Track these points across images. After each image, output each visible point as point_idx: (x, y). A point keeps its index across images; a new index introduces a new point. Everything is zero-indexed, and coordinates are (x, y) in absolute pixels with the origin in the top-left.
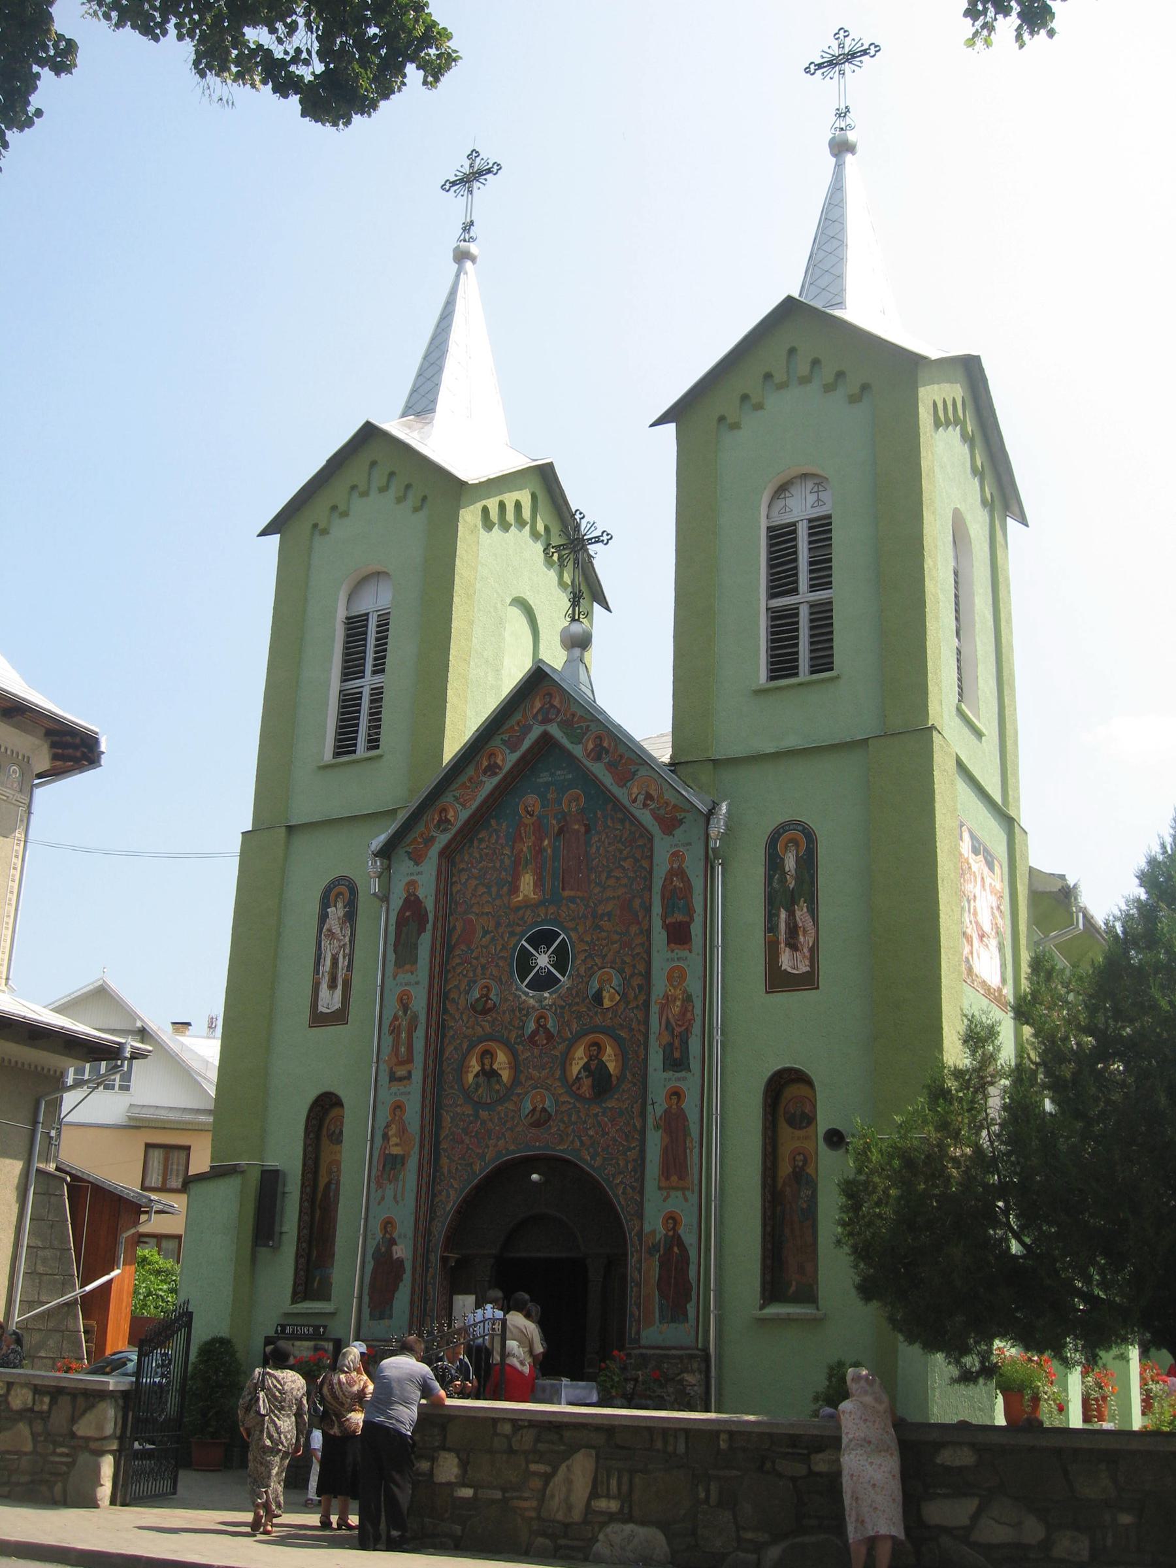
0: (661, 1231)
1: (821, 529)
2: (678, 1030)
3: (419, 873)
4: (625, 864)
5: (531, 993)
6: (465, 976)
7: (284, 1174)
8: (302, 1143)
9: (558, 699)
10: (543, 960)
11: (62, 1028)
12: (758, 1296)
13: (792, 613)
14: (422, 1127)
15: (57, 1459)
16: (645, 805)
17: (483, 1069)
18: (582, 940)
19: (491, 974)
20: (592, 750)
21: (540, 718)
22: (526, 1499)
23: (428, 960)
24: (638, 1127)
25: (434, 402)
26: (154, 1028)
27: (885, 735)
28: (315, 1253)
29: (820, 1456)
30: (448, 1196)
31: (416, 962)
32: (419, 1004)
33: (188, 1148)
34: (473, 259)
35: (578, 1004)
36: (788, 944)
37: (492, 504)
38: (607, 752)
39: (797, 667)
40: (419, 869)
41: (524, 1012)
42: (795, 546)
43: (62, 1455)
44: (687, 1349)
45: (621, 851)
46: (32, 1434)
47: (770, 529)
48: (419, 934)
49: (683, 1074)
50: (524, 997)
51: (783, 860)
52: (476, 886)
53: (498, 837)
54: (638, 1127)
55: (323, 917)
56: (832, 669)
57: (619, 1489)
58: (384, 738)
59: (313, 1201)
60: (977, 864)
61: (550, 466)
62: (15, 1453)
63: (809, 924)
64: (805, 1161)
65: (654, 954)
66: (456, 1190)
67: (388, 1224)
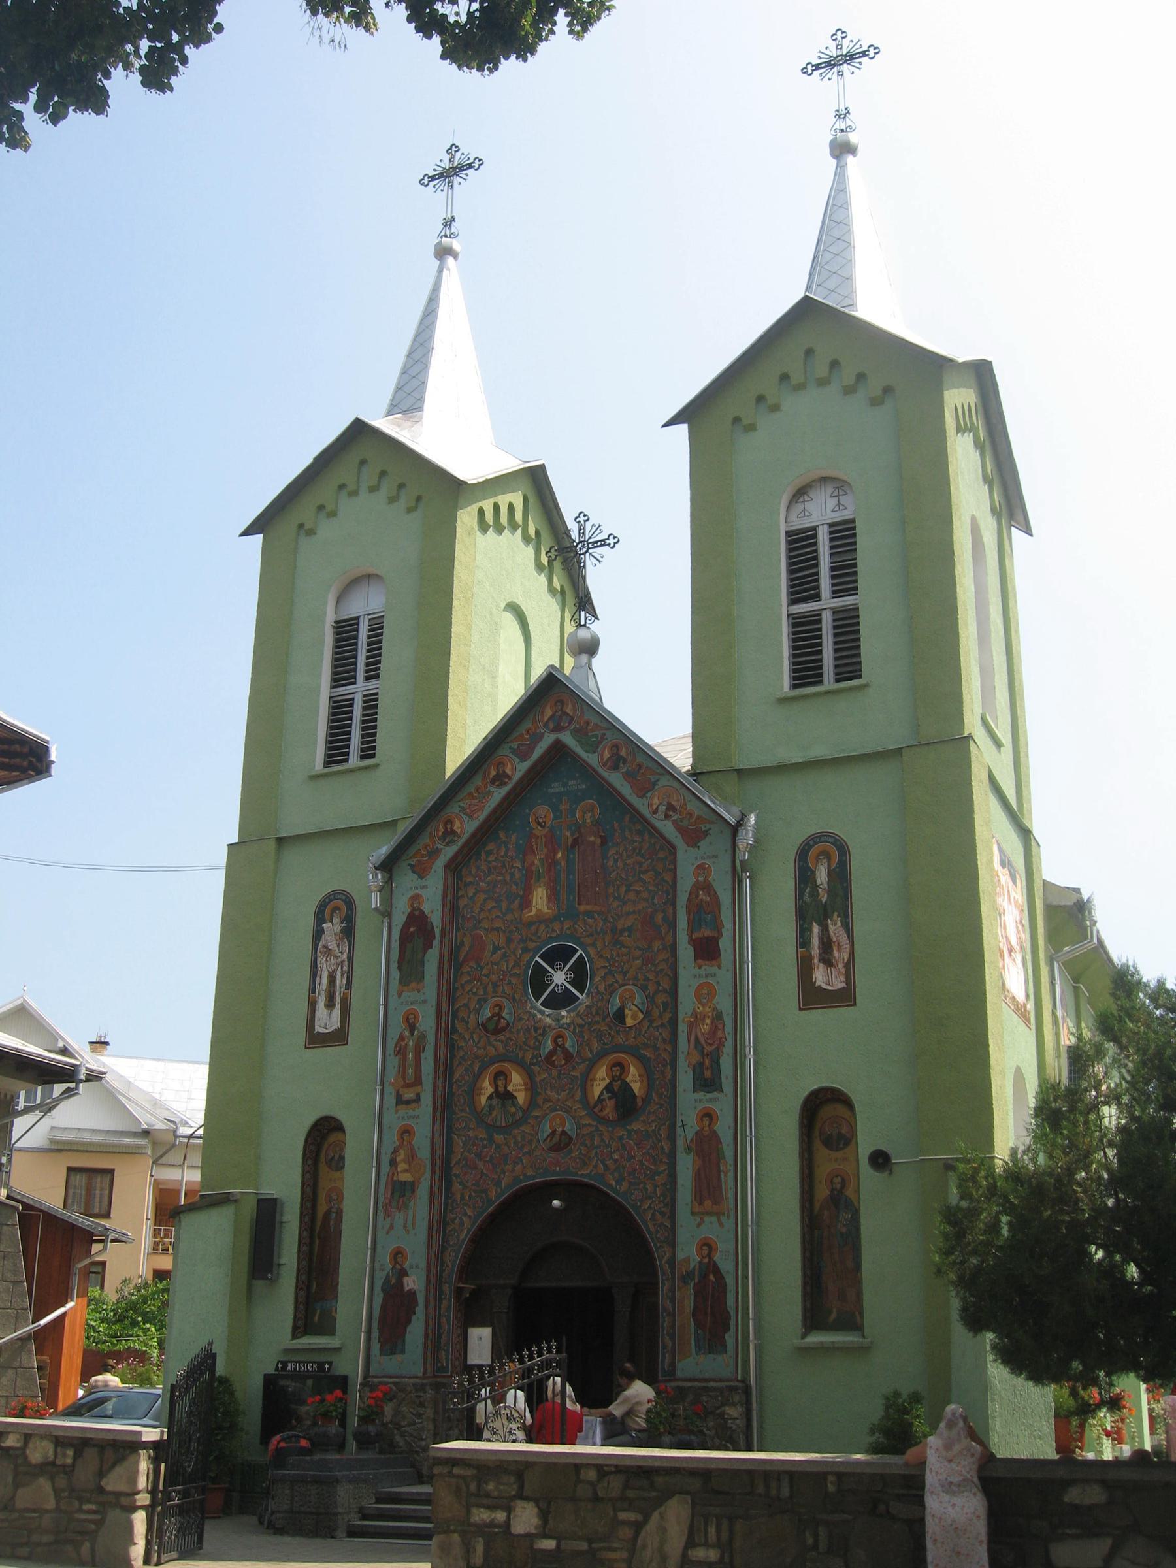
2: (708, 1049)
3: (423, 887)
5: (548, 1011)
6: (475, 994)
7: (282, 1204)
10: (559, 977)
11: (16, 1050)
13: (815, 619)
15: (84, 1516)
16: (667, 817)
18: (601, 956)
20: (609, 759)
21: (551, 725)
22: (615, 1550)
23: (435, 978)
24: (667, 1151)
25: (421, 400)
26: (76, 1047)
27: (919, 745)
31: (422, 979)
32: (427, 1024)
33: (111, 1172)
34: (455, 256)
35: (597, 1022)
37: (487, 505)
38: (625, 761)
39: (821, 675)
42: (816, 551)
43: (89, 1512)
44: (728, 1380)
45: (640, 864)
46: (55, 1490)
49: (716, 1094)
50: (539, 1016)
51: (814, 872)
52: (485, 899)
53: (507, 850)
54: (667, 1151)
55: (318, 933)
56: (860, 677)
59: (311, 1230)
60: (1004, 877)
62: (34, 1511)
63: (844, 938)
65: (681, 972)
67: (398, 1254)
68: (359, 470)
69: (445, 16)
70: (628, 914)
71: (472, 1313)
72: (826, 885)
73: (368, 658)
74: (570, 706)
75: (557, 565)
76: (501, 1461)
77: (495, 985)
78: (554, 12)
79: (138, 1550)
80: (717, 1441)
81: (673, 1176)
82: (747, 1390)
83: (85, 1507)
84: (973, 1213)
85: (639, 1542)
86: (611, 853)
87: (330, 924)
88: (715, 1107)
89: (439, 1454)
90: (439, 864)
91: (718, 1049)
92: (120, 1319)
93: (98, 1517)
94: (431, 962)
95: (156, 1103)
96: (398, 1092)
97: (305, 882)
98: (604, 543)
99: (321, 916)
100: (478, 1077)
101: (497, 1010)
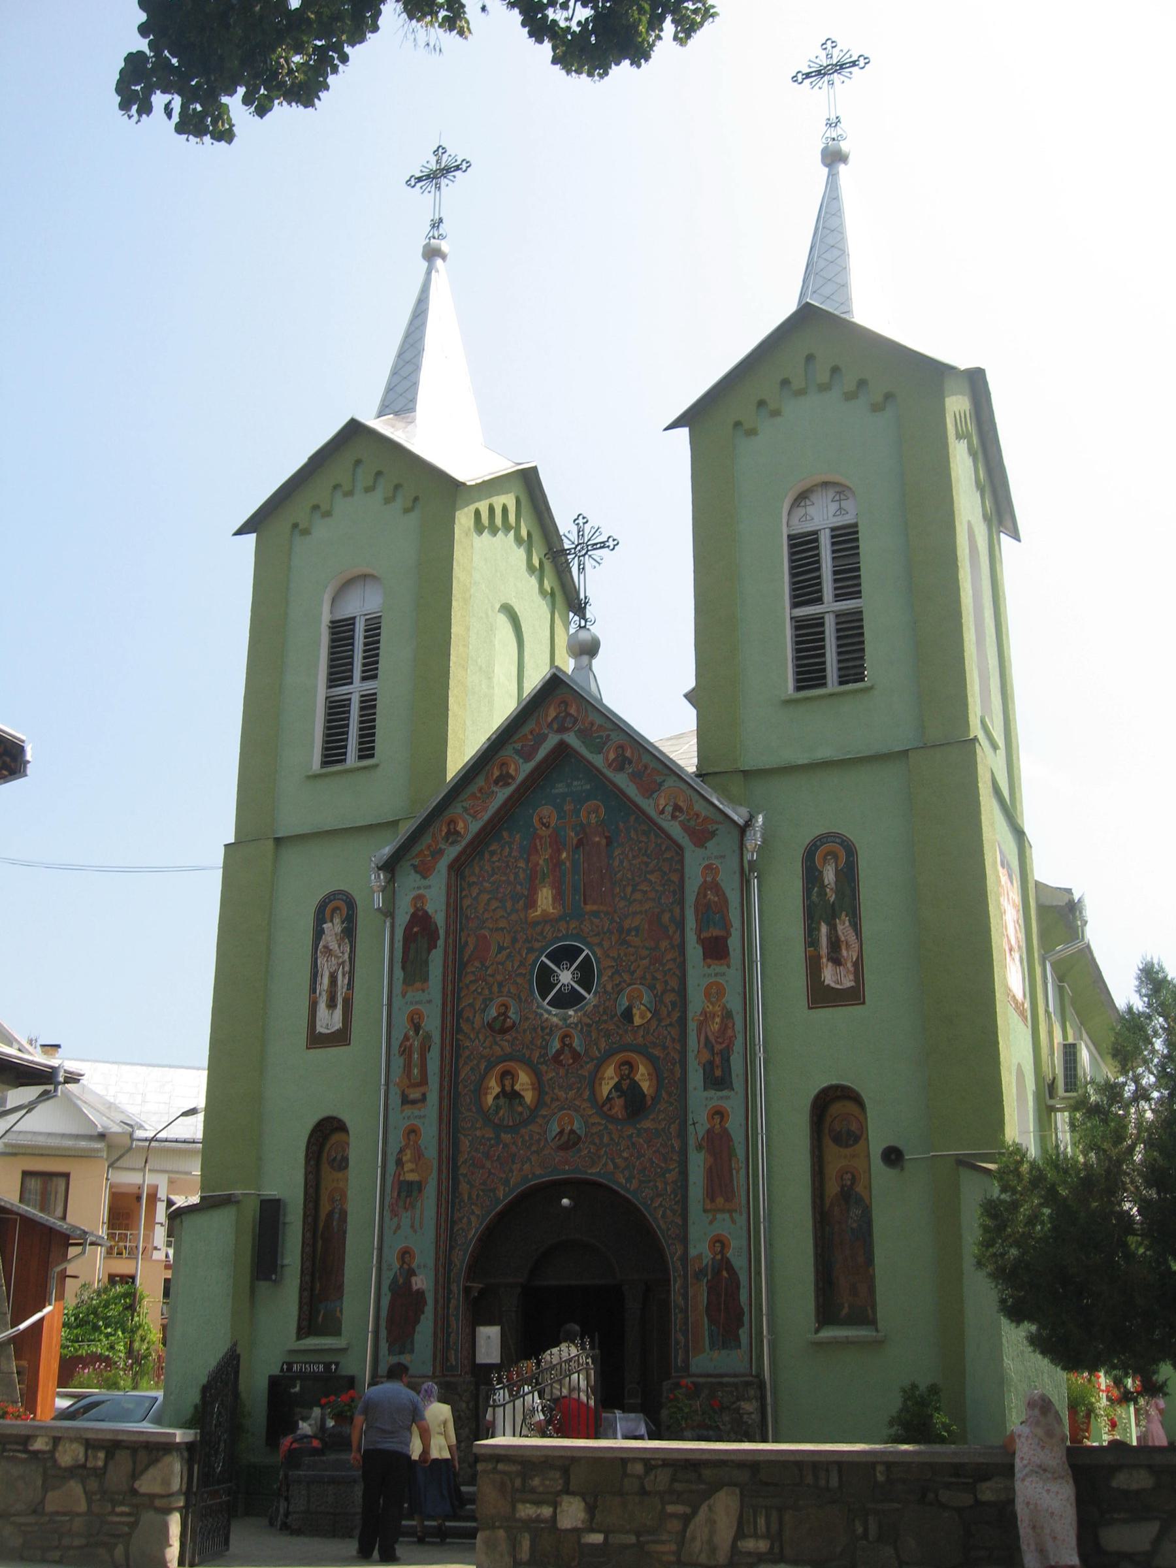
1: (846, 539)
2: (718, 1048)
3: (429, 887)
4: (652, 878)
5: (554, 1011)
6: (480, 994)
8: (303, 1171)
10: (566, 977)
12: (813, 1318)
13: (818, 623)
14: (440, 1151)
16: (674, 817)
17: (503, 1091)
18: (608, 956)
19: (509, 991)
20: (613, 760)
21: (555, 726)
22: (663, 1542)
23: (440, 978)
25: (413, 400)
29: (988, 1484)
30: (470, 1222)
32: (432, 1024)
33: (67, 1176)
34: (444, 257)
35: (605, 1022)
37: (483, 506)
39: (825, 677)
40: (426, 882)
42: (818, 555)
43: (122, 1514)
44: (743, 1375)
45: (647, 864)
46: (85, 1492)
47: (791, 537)
48: (429, 952)
49: (725, 1093)
50: (546, 1016)
51: (821, 873)
55: (319, 933)
57: (768, 1528)
58: (379, 745)
61: (534, 470)
62: (65, 1514)
63: (852, 938)
64: (854, 1179)
65: (690, 972)
66: (478, 1216)
68: (354, 470)
69: (554, 22)
70: (635, 913)
71: (480, 1314)
72: (833, 885)
73: (365, 658)
75: (548, 566)
76: (547, 1457)
77: (500, 985)
78: (661, 19)
79: (173, 1552)
80: (732, 1435)
81: (684, 1173)
82: (761, 1385)
83: (119, 1509)
84: (1014, 1206)
88: (726, 1104)
89: (483, 1451)
91: (728, 1047)
92: (81, 1323)
93: (132, 1519)
94: (436, 959)
95: (111, 1106)
96: (403, 1093)
97: (303, 884)
98: (603, 545)
99: (321, 916)
100: (484, 1077)
101: (502, 1010)
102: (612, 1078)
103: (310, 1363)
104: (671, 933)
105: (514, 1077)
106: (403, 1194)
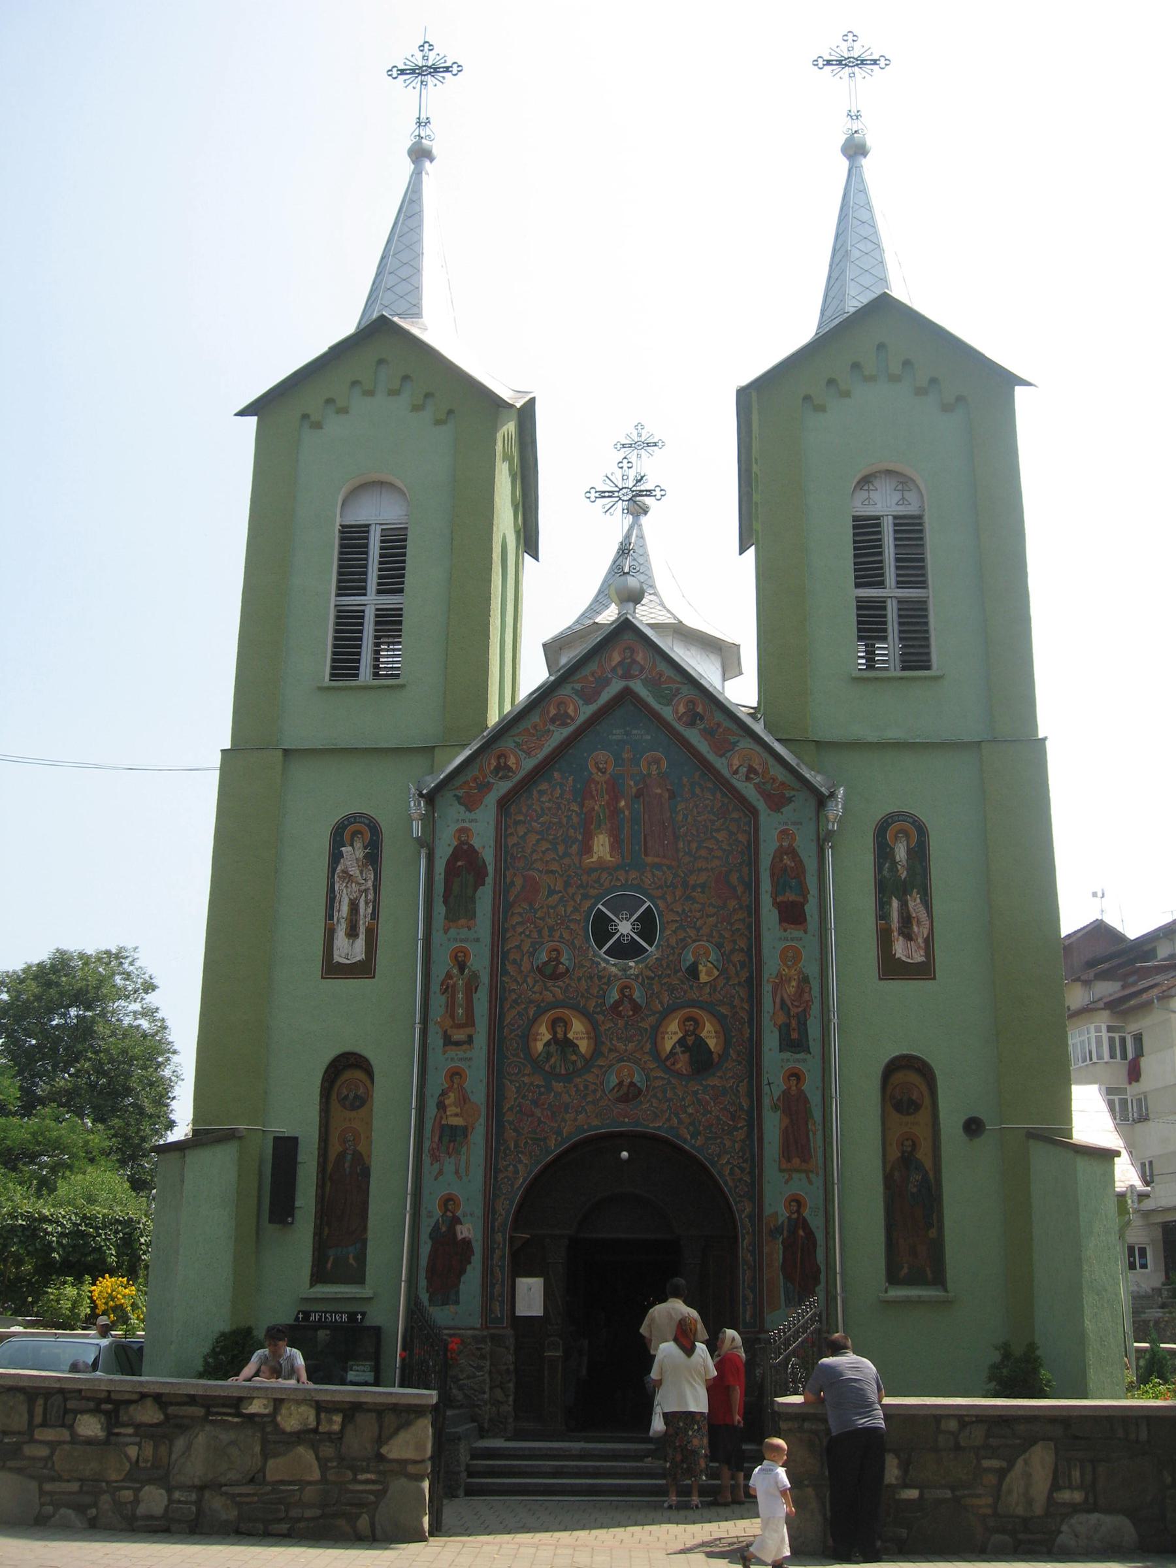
0: (783, 1214)
2: (794, 1011)
3: (475, 821)
5: (613, 961)
9: (641, 655)
10: (625, 928)
16: (748, 779)
18: (672, 910)
19: (561, 936)
21: (620, 672)
22: (979, 1496)
28: (326, 1230)
30: (516, 1172)
31: (473, 916)
32: (480, 962)
35: (669, 976)
36: (901, 933)
41: (605, 980)
43: (367, 1482)
46: (317, 1458)
48: (475, 891)
50: (603, 965)
52: (538, 841)
55: (335, 857)
56: (928, 668)
62: (291, 1483)
63: (923, 915)
64: (914, 1145)
67: (448, 1202)
71: (522, 1264)
72: (905, 863)
74: (641, 655)
77: (551, 929)
85: (1004, 1487)
86: (679, 808)
87: (350, 848)
89: (782, 1410)
90: (491, 799)
93: (380, 1487)
96: (445, 1032)
97: (315, 806)
99: (340, 835)
101: (554, 954)
102: (676, 1033)
103: (336, 1313)
104: (739, 893)
105: (567, 1025)
106: (446, 1139)
